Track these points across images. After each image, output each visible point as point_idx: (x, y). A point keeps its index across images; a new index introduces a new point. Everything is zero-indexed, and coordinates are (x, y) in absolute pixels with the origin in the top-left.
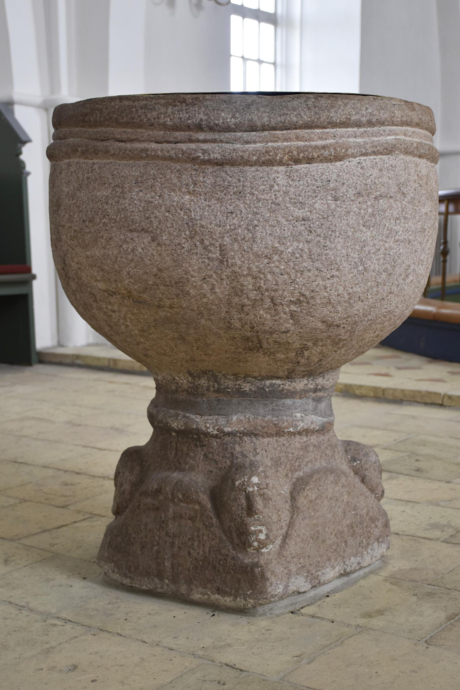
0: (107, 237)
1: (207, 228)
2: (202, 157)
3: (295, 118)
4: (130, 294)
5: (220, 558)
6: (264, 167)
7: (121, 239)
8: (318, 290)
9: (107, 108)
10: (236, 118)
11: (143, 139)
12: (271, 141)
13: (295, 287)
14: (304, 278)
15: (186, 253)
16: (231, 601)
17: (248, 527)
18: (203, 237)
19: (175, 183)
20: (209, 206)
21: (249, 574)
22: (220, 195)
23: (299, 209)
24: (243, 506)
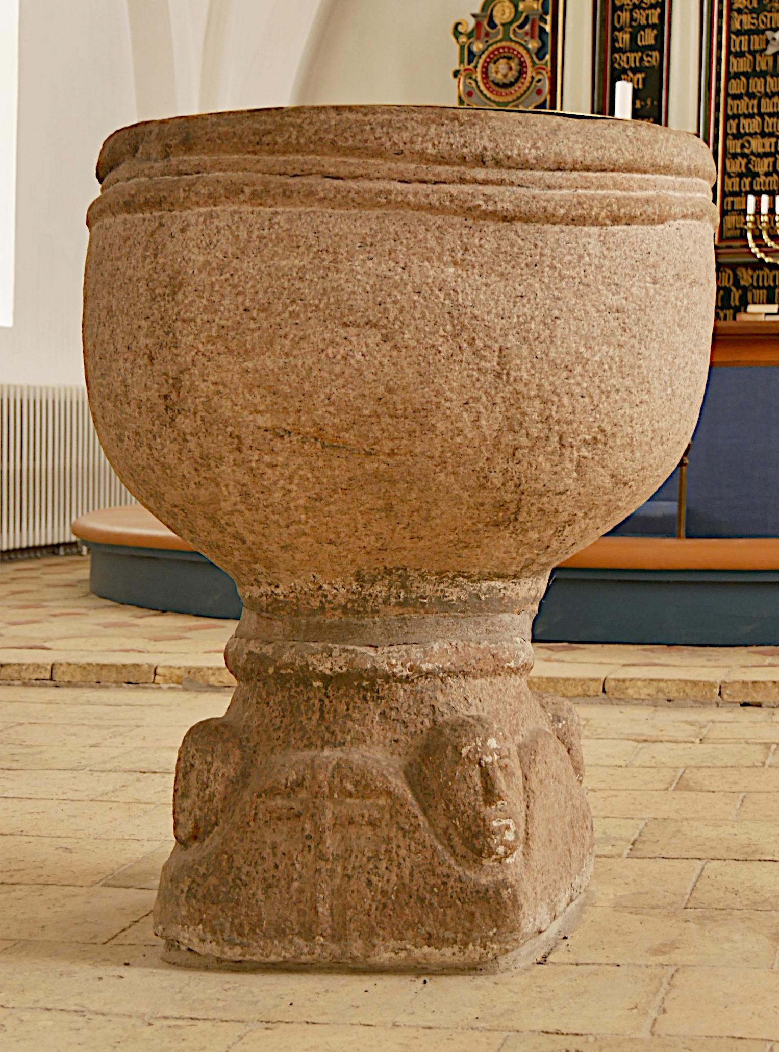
0: (295, 336)
1: (483, 320)
2: (483, 207)
3: (615, 155)
4: (321, 432)
5: (432, 883)
6: (572, 227)
7: (325, 340)
8: (622, 423)
9: (311, 123)
10: (538, 148)
11: (377, 175)
12: (582, 187)
13: (595, 418)
14: (609, 404)
15: (443, 361)
16: (454, 954)
17: (487, 823)
18: (474, 335)
19: (431, 248)
20: (486, 285)
21: (491, 901)
22: (505, 268)
23: (613, 295)
24: (477, 788)
